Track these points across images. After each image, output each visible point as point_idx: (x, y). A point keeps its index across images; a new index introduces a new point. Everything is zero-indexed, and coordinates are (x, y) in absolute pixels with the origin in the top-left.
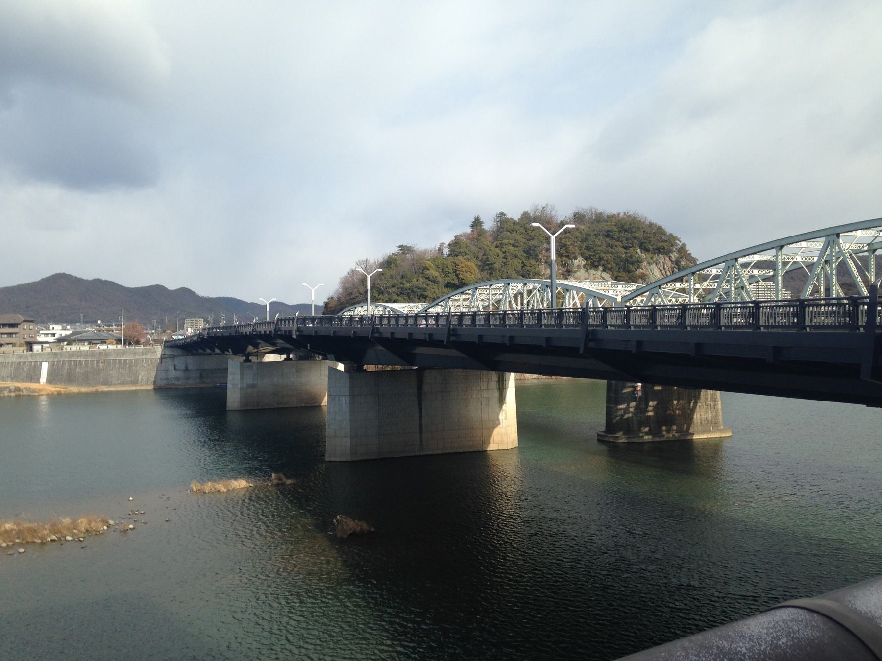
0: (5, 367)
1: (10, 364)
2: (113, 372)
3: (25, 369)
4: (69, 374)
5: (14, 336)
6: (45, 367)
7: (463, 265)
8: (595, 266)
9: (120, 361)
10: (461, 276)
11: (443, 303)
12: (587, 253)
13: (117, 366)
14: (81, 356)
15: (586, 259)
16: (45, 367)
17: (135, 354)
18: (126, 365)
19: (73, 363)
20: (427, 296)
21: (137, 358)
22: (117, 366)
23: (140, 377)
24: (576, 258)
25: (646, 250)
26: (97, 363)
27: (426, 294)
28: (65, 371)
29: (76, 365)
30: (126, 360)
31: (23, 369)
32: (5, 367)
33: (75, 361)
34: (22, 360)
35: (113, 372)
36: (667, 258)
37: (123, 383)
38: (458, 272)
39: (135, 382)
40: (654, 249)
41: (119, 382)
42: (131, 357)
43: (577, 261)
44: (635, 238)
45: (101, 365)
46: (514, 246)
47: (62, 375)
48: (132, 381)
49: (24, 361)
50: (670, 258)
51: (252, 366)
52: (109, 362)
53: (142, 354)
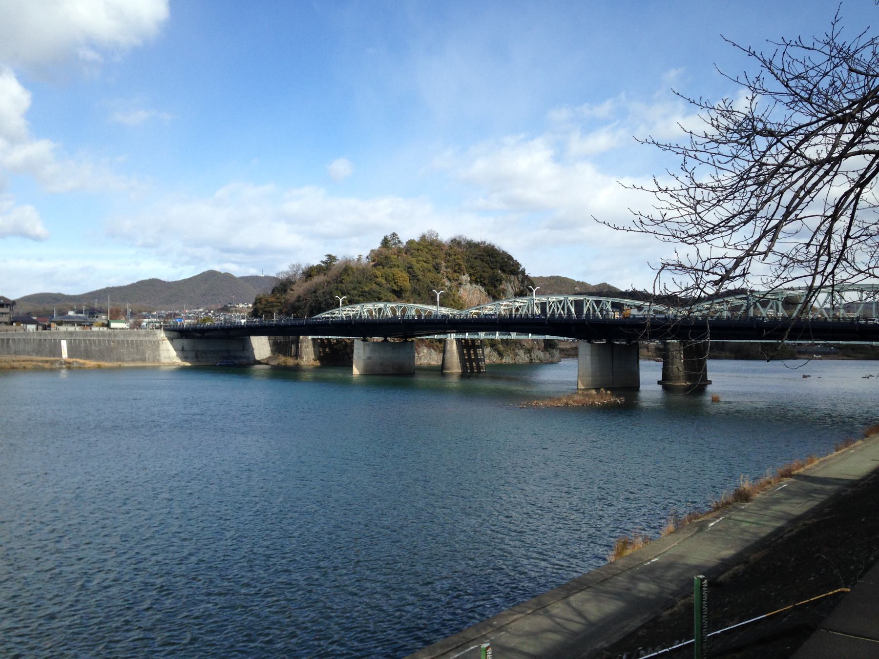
0: (28, 342)
1: (32, 340)
2: (124, 351)
3: (47, 346)
4: (86, 351)
5: (4, 315)
6: (64, 343)
7: (400, 276)
8: (476, 282)
9: (127, 341)
10: (399, 284)
11: (688, 308)
12: (472, 271)
13: (126, 345)
14: (93, 336)
15: (470, 275)
16: (64, 343)
17: (139, 335)
18: (133, 344)
19: (87, 341)
20: (381, 298)
21: (141, 339)
22: (126, 345)
23: (147, 355)
24: (464, 274)
25: (504, 271)
26: (108, 342)
27: (381, 296)
28: (82, 349)
29: (90, 343)
30: (132, 341)
31: (45, 345)
32: (28, 342)
33: (89, 340)
34: (42, 338)
35: (124, 351)
36: (516, 278)
37: (133, 360)
38: (396, 281)
39: (144, 360)
40: (509, 271)
41: (130, 359)
42: (136, 338)
43: (465, 276)
44: (497, 262)
45: (112, 344)
46: (425, 262)
47: (80, 351)
48: (140, 359)
49: (45, 338)
50: (518, 278)
51: (369, 344)
52: (118, 341)
53: (145, 336)
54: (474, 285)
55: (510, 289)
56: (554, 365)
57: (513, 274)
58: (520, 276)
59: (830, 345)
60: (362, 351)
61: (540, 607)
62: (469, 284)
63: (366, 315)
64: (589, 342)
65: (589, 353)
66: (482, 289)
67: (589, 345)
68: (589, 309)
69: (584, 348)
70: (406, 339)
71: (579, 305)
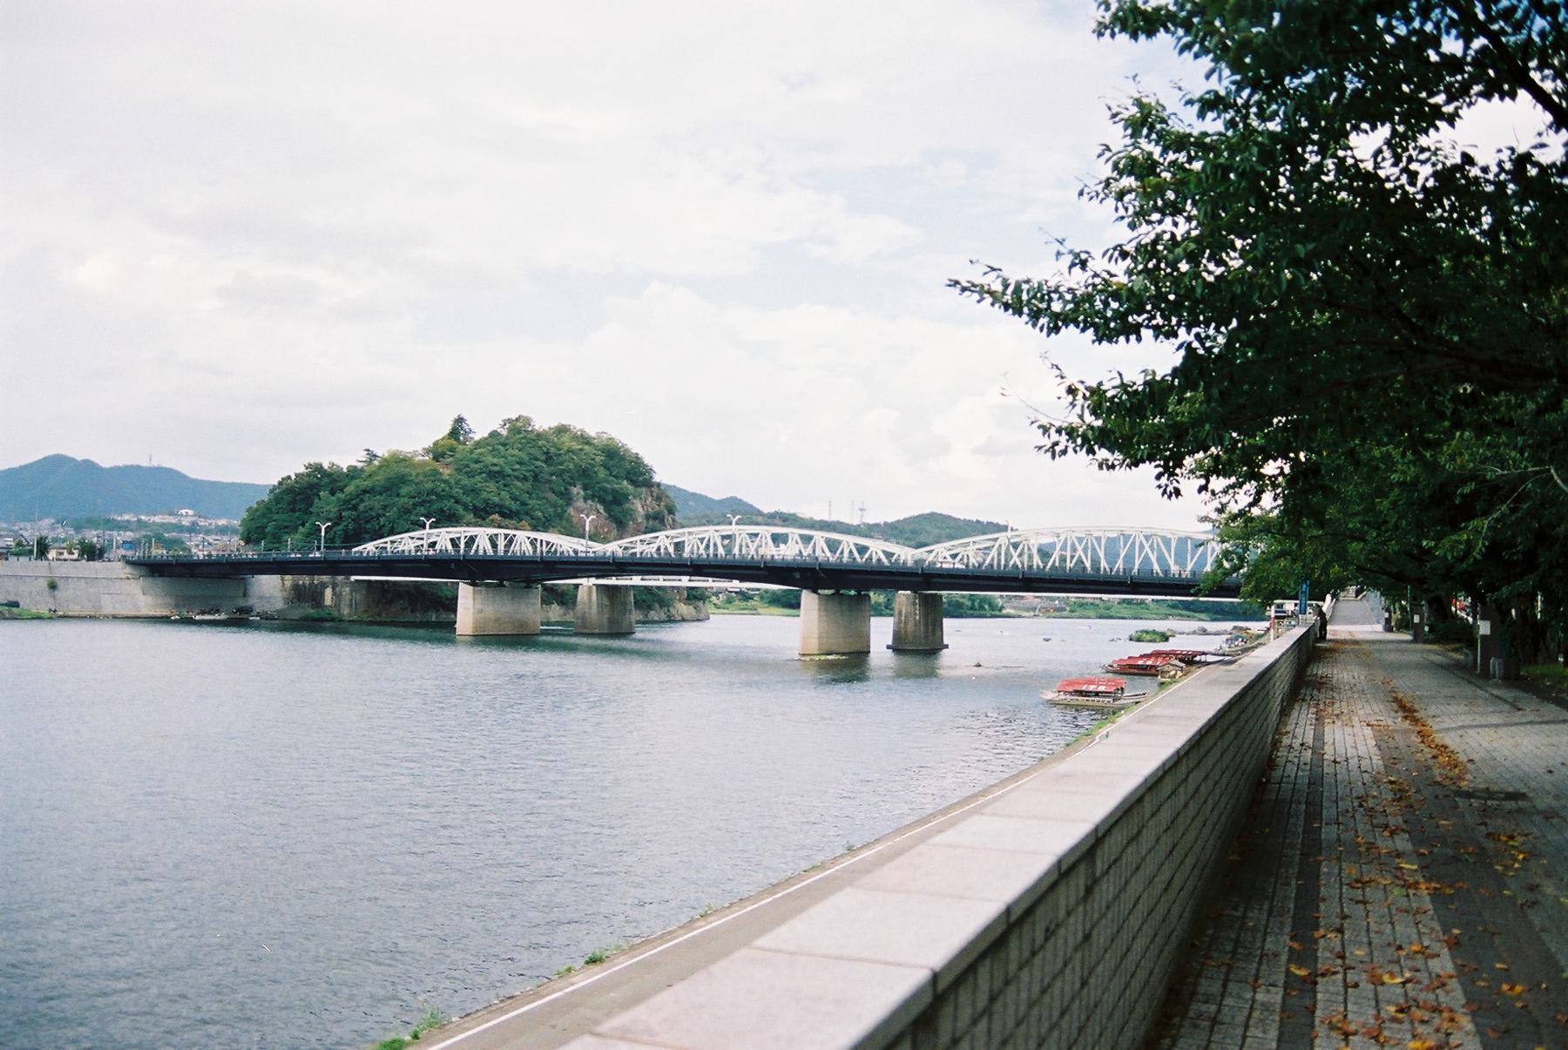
25: (633, 482)
50: (652, 492)
54: (590, 502)
55: (640, 509)
56: (700, 624)
57: (646, 486)
58: (655, 489)
59: (1053, 599)
60: (472, 601)
61: (1540, 720)
62: (582, 500)
63: (620, 553)
64: (815, 591)
65: (817, 607)
66: (601, 508)
67: (816, 596)
68: (993, 559)
69: (808, 598)
70: (501, 581)
71: (833, 546)
